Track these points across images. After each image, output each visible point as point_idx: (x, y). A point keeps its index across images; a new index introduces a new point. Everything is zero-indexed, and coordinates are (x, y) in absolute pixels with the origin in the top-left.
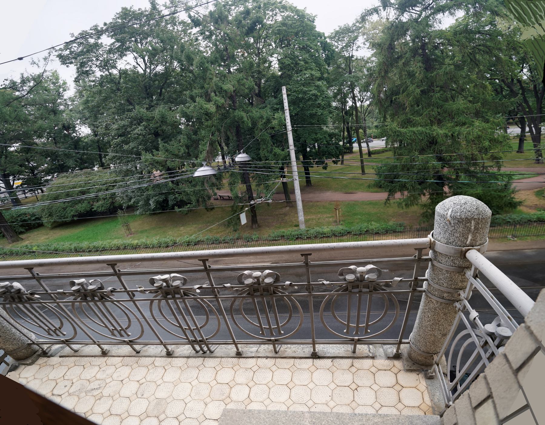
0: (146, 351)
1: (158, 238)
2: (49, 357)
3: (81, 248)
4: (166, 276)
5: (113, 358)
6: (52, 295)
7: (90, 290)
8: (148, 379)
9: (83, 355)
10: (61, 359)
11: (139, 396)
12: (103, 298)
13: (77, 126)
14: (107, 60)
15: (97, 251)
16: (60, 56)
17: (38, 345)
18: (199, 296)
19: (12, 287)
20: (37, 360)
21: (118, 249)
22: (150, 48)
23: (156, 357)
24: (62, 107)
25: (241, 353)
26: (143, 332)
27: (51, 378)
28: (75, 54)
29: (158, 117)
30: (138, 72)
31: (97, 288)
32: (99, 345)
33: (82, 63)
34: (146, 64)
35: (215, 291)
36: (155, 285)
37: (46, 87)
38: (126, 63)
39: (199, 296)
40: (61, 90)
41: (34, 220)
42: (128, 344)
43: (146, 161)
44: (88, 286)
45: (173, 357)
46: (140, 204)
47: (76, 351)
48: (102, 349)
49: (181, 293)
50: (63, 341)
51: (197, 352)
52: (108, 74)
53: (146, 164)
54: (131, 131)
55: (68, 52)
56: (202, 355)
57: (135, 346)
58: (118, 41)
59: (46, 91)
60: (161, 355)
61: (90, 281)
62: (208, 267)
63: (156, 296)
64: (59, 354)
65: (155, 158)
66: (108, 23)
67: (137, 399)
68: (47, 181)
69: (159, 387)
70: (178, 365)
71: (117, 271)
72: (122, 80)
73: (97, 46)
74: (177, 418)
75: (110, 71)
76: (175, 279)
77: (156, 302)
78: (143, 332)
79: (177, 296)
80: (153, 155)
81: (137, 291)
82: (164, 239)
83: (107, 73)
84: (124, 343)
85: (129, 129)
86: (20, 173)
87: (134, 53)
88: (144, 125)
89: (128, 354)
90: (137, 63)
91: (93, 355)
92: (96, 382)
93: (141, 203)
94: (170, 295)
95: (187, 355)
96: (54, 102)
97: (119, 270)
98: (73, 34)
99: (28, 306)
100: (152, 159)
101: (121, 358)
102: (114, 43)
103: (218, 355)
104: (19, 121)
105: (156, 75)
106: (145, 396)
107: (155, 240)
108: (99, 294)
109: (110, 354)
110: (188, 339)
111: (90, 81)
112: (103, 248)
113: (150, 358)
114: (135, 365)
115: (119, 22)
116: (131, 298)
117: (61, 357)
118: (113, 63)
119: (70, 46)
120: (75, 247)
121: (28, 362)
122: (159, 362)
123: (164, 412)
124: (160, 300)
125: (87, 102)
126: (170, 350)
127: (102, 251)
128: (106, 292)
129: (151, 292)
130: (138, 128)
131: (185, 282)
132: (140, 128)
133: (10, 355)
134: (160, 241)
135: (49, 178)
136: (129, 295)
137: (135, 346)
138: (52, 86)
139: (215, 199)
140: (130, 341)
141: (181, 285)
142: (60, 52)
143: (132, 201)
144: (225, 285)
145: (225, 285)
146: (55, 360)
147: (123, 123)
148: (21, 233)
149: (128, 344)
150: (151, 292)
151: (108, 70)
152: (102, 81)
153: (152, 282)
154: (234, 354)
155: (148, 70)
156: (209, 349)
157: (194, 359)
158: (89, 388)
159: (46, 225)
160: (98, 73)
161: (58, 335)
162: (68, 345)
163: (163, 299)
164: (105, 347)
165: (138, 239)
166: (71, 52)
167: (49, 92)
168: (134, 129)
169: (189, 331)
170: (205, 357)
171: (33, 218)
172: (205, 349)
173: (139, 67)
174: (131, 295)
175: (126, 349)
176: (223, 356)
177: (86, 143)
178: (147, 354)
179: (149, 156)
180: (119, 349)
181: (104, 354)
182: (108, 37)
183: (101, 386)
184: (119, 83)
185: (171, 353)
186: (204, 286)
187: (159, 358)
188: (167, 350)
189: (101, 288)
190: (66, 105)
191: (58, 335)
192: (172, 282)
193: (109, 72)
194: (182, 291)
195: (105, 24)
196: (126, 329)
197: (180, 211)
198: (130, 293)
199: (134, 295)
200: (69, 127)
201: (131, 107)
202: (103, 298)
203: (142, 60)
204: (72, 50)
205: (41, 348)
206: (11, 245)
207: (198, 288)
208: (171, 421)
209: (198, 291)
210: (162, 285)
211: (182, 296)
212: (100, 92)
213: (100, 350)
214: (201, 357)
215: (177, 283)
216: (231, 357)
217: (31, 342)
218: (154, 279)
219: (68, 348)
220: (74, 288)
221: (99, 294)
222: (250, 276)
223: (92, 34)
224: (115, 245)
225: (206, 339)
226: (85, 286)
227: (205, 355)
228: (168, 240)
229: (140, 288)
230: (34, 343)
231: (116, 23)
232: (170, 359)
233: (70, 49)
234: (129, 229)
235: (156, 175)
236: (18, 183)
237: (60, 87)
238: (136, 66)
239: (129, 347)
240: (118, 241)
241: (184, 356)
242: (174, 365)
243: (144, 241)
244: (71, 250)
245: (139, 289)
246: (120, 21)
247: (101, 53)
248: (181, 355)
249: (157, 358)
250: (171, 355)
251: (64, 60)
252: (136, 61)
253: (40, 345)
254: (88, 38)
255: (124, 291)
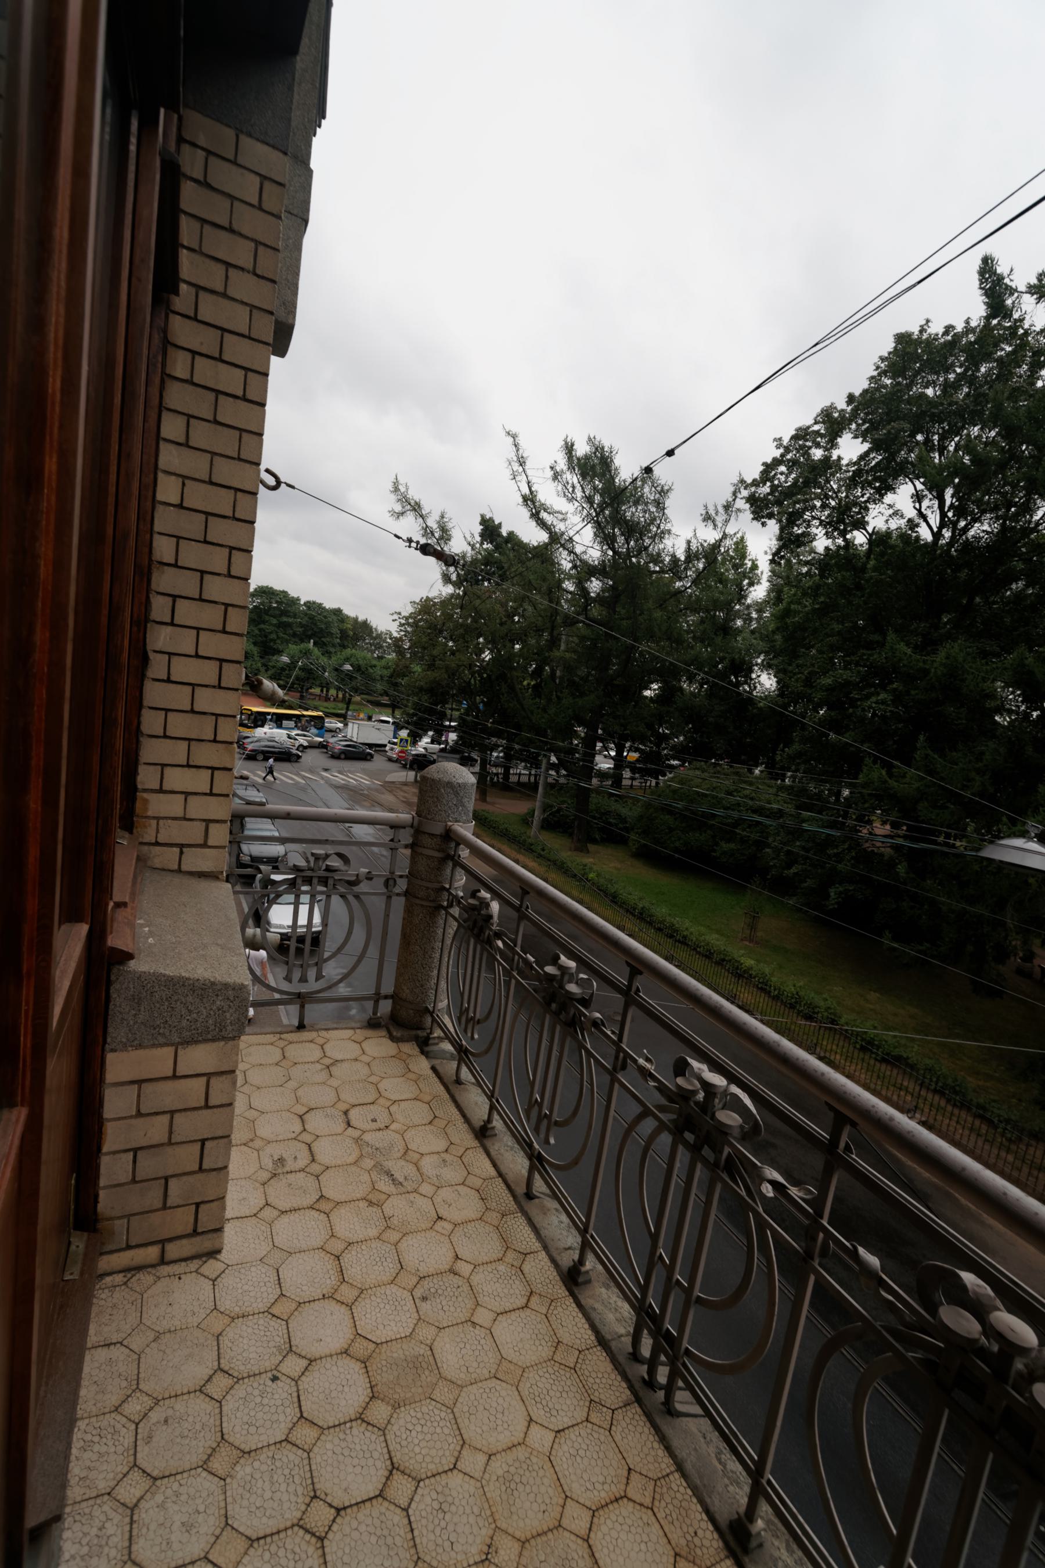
0: (545, 1211)
1: (801, 984)
2: (422, 1052)
3: (651, 916)
4: (718, 1080)
5: (485, 1155)
6: (516, 957)
7: (568, 992)
8: (475, 1279)
9: (458, 1098)
10: (430, 1072)
11: (418, 1293)
12: (573, 1024)
13: (756, 668)
14: (847, 503)
15: (671, 936)
16: (752, 500)
17: (434, 1020)
18: (761, 1210)
19: (488, 905)
20: (407, 1041)
21: (707, 957)
22: (967, 460)
23: (545, 1248)
24: (739, 623)
25: (754, 1543)
26: (576, 1162)
27: (381, 1086)
28: (781, 493)
29: (939, 673)
30: (918, 538)
31: (579, 997)
32: (492, 1108)
33: (790, 514)
34: (943, 515)
35: (814, 1239)
36: (680, 1081)
37: (723, 574)
38: (891, 511)
39: (761, 1210)
40: (746, 582)
41: (620, 829)
42: (530, 1157)
43: (865, 785)
44: (570, 982)
45: (572, 1294)
46: (806, 885)
47: (458, 1081)
48: (489, 1120)
49: (721, 1152)
50: (461, 1046)
51: (635, 1356)
52: (843, 543)
53: (865, 791)
54: (858, 700)
55: (766, 489)
56: (638, 1385)
57: (537, 1176)
58: (876, 447)
59: (721, 582)
60: (558, 1258)
61: (582, 976)
62: (842, 1145)
63: (661, 1108)
64: (436, 1062)
65: (892, 783)
66: (857, 393)
67: (406, 1294)
68: (672, 767)
69: (468, 1327)
70: (560, 1333)
71: (634, 989)
72: (872, 563)
73: (828, 465)
74: (394, 1468)
75: (848, 536)
76: (736, 1105)
77: (648, 1125)
78: (576, 1162)
79: (706, 1151)
80: (890, 775)
81: (635, 1061)
82: (812, 995)
83: (840, 541)
84: (527, 1146)
85: (855, 695)
86: (643, 739)
87: (917, 483)
88: (895, 690)
89: (510, 1177)
90: (919, 511)
91: (468, 1115)
92: (411, 1166)
93: (809, 883)
94: (692, 1133)
95: (605, 1331)
96: (728, 607)
97: (638, 990)
98: (780, 439)
99: (479, 947)
100: (885, 782)
101: (492, 1172)
102: (867, 454)
103: (676, 1443)
104: (669, 639)
105: (969, 547)
106: (425, 1307)
107: (791, 983)
108: (572, 1011)
109: (488, 1143)
110: (644, 1290)
111: (800, 563)
112: (685, 937)
113: (532, 1236)
114: (493, 1217)
115: (885, 386)
116: (615, 1069)
117: (434, 1069)
118: (859, 513)
119: (773, 473)
120: (642, 908)
121: (395, 1034)
122: (540, 1268)
123: (396, 1406)
124: (662, 1127)
125: (787, 613)
126: (583, 1269)
127: (679, 941)
128: (585, 1016)
129: (661, 1088)
130: (878, 694)
131: (751, 1133)
132: (883, 696)
133: (394, 1002)
134: (802, 993)
135: (675, 762)
136: (617, 1058)
137: (537, 1176)
138: (731, 575)
139: (1019, 971)
140: (540, 1158)
141: (736, 1133)
142: (753, 489)
143: (794, 870)
144: (861, 1250)
145: (861, 1250)
146: (423, 1065)
147: (847, 675)
148: (594, 841)
149: (530, 1159)
150: (661, 1088)
151: (843, 534)
152: (828, 562)
153: (681, 1068)
154: (725, 1513)
155: (947, 534)
156: (669, 1389)
157: (609, 1367)
158: (389, 1164)
159: (631, 844)
160: (821, 543)
161: (465, 1031)
162: (460, 1061)
163: (670, 1132)
164: (497, 1123)
165: (758, 961)
166: (774, 488)
167: (725, 586)
168: (868, 697)
169: (664, 1274)
170: (639, 1400)
171: (621, 825)
172: (662, 1375)
173: (923, 525)
174: (622, 1062)
175: (518, 1164)
176: (688, 1466)
177: (761, 709)
178: (537, 1219)
179: (878, 773)
180: (512, 1149)
181: (482, 1133)
182: (856, 437)
183: (405, 1184)
184: (863, 569)
185: (581, 1280)
186: (794, 1192)
187: (546, 1259)
188: (581, 1261)
189: (586, 1002)
190: (748, 619)
191: (465, 1031)
192: (720, 1106)
193: (845, 540)
194: (727, 1150)
195: (851, 398)
196: (556, 1123)
197: (895, 949)
198: (622, 1055)
199: (624, 1067)
200: (743, 669)
201: (876, 637)
202: (573, 1024)
203: (936, 503)
204: (776, 482)
205: (431, 1029)
206: (569, 853)
207: (774, 1183)
208: (376, 1455)
209: (768, 1190)
210: (694, 1092)
211: (716, 1165)
212: (816, 590)
213: (486, 1117)
214: (631, 1387)
215: (730, 1118)
216: (707, 1511)
217: (431, 1009)
218: (688, 1064)
219: (454, 1064)
220: (550, 969)
221: (572, 1011)
222: (979, 1310)
223: (817, 433)
224: (708, 944)
225: (687, 1352)
226: (566, 978)
227: (643, 1392)
228: (822, 1003)
229: (648, 1060)
230: (431, 1013)
231: (877, 389)
232: (561, 1291)
233: (772, 480)
234: (752, 927)
235: (878, 831)
236: (634, 756)
237: (744, 575)
238: (917, 520)
239: (526, 1163)
240: (718, 940)
241: (597, 1322)
242: (552, 1318)
243: (767, 970)
244: (635, 909)
245: (641, 1061)
246: (888, 382)
247: (835, 486)
248: (593, 1315)
249: (543, 1255)
250: (576, 1284)
251: (760, 509)
252: (917, 505)
253: (435, 1025)
254: (810, 448)
255: (613, 1042)
